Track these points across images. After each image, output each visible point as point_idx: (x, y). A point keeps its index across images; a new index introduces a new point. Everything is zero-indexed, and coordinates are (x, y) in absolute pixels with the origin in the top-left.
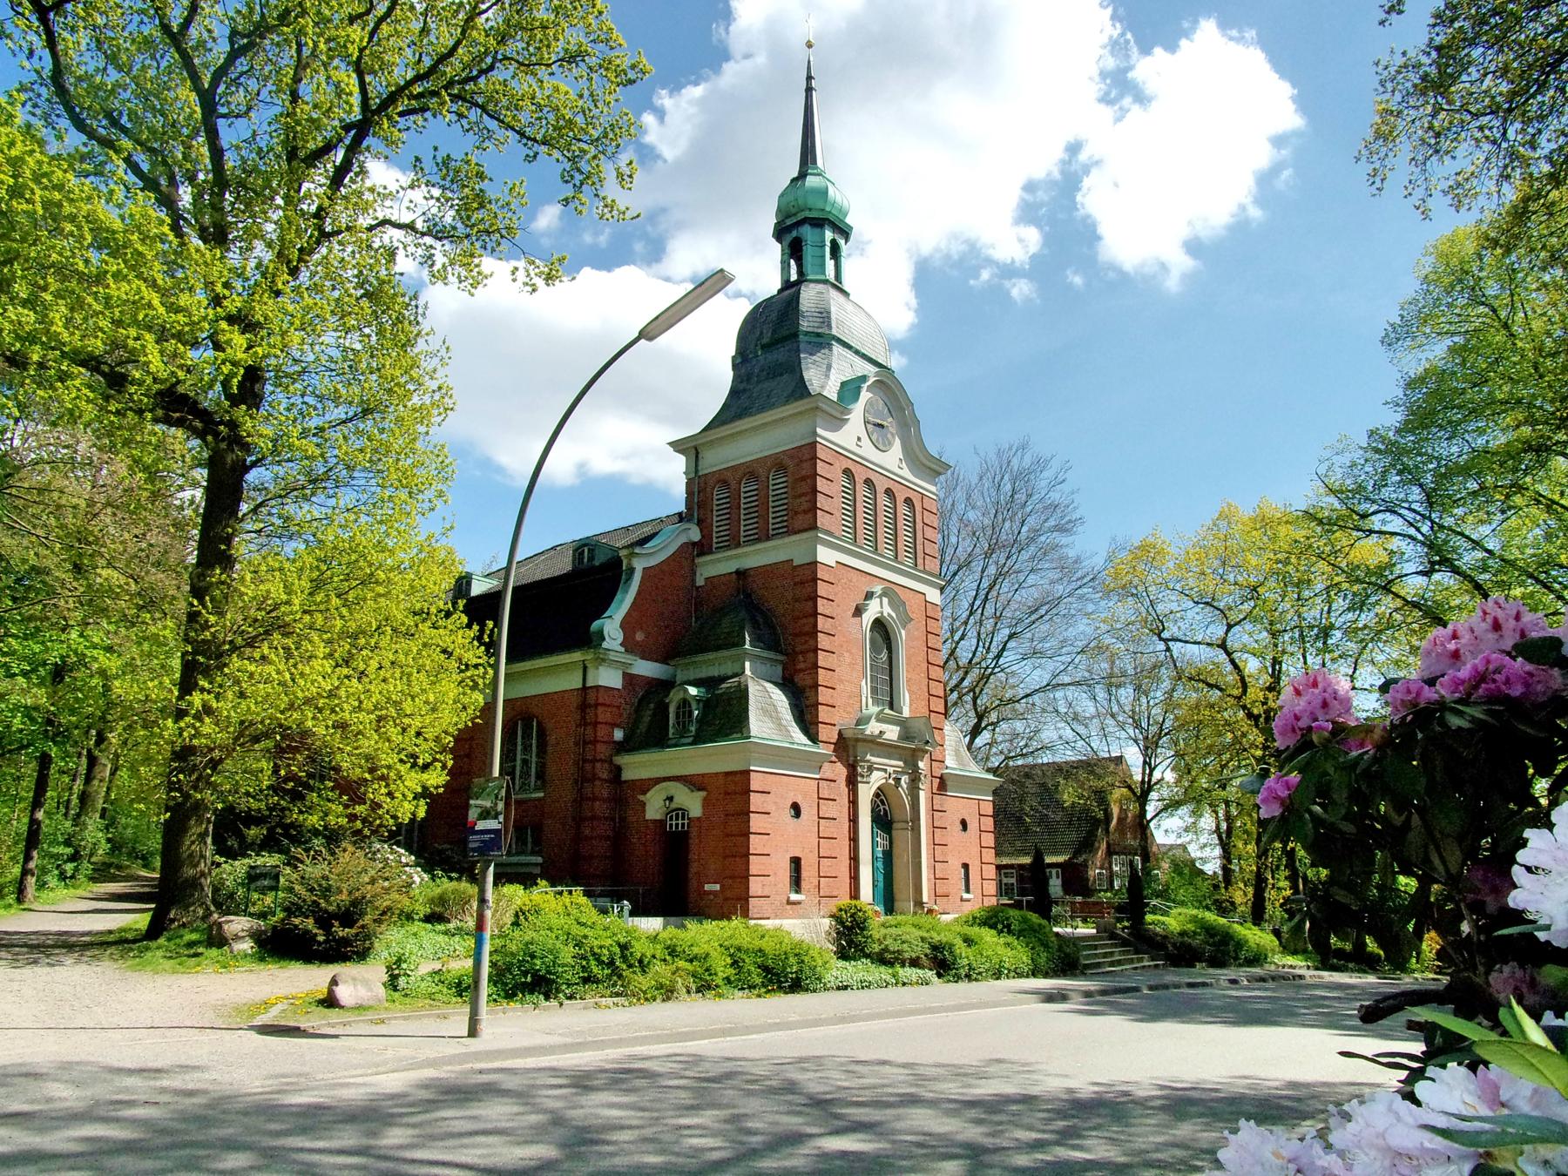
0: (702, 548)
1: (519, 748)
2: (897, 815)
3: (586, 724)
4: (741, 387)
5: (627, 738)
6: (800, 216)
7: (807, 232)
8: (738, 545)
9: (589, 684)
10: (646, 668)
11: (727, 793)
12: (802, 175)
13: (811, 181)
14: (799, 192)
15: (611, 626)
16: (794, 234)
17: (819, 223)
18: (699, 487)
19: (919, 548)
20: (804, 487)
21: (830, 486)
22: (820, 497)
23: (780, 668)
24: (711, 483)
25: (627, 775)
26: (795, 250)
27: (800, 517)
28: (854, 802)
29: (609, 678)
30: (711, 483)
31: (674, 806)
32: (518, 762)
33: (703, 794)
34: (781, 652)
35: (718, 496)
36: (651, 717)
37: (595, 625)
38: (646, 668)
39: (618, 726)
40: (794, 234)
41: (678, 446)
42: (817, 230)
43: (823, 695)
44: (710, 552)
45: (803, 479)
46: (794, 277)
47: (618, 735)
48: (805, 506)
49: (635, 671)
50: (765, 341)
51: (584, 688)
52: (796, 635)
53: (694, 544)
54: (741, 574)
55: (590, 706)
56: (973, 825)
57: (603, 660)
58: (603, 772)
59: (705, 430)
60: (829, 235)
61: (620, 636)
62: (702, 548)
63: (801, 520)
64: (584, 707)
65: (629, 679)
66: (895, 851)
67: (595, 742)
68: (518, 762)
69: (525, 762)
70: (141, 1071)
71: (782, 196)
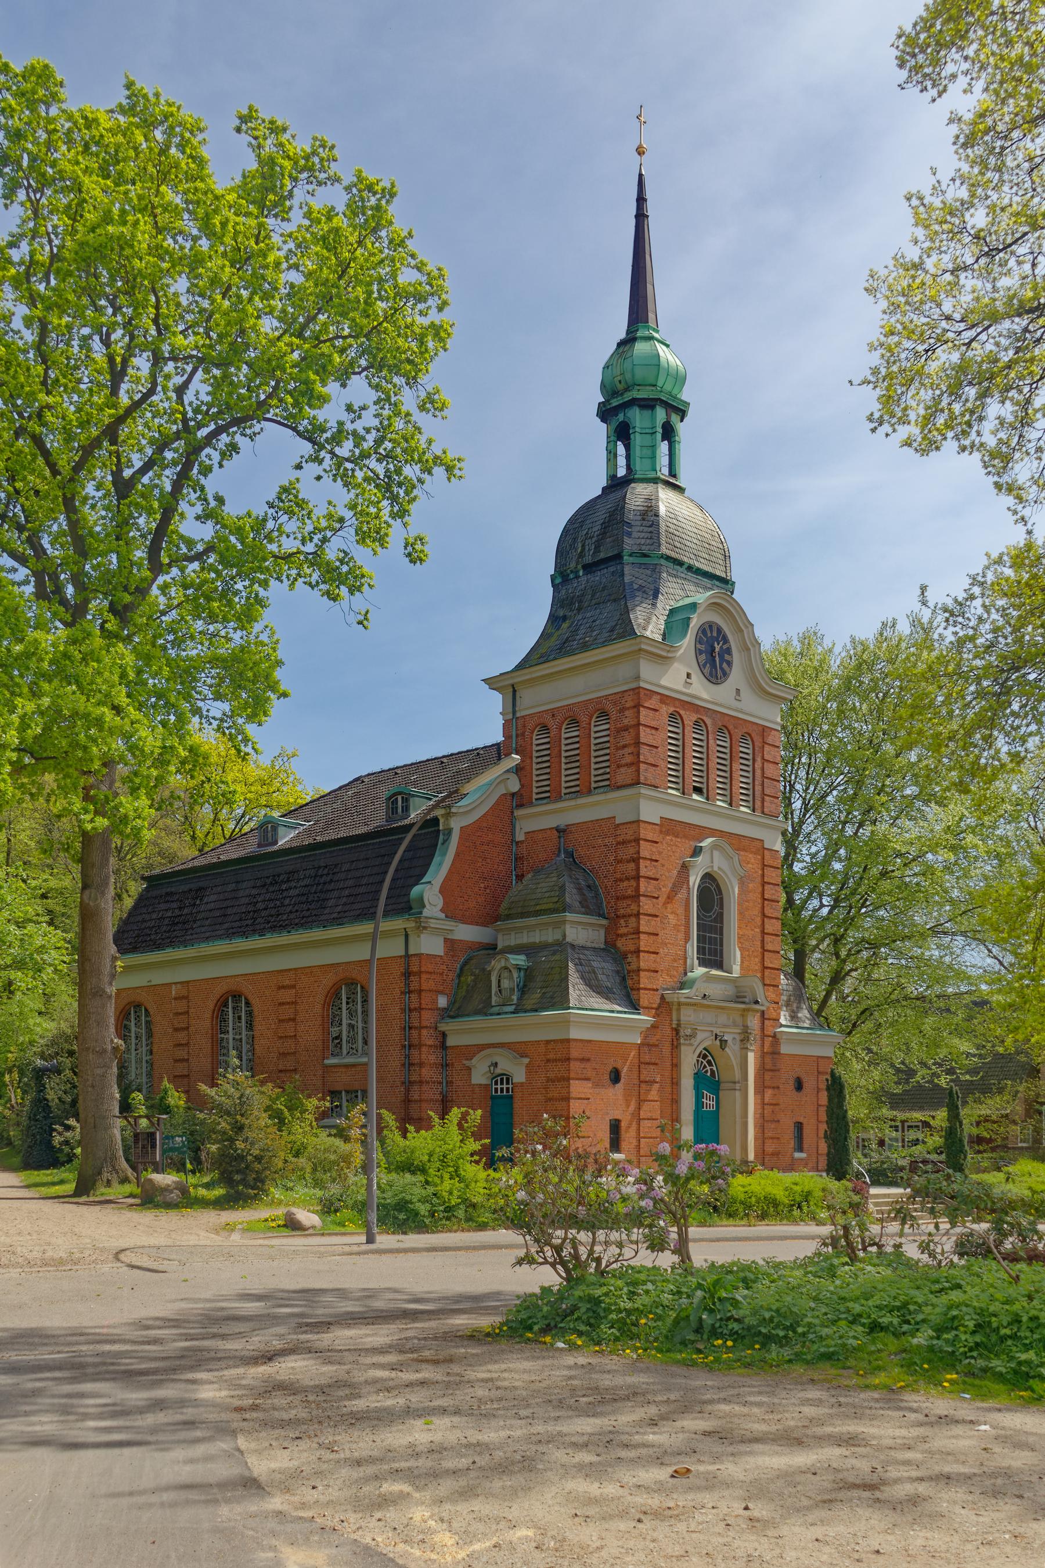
0: (519, 800)
1: (344, 1012)
2: (724, 1076)
3: (410, 992)
4: (561, 613)
5: (452, 1003)
6: (628, 396)
7: (637, 418)
8: (559, 798)
9: (411, 952)
10: (467, 933)
11: (548, 1061)
12: (628, 342)
13: (640, 347)
14: (627, 365)
15: (430, 892)
16: (621, 417)
17: (648, 405)
18: (517, 727)
19: (758, 788)
20: (627, 738)
21: (657, 734)
22: (644, 750)
23: (602, 932)
24: (530, 726)
25: (451, 1042)
26: (622, 433)
27: (623, 770)
28: (676, 1066)
29: (430, 945)
30: (530, 726)
31: (498, 1071)
32: (344, 1027)
33: (526, 1061)
34: (602, 915)
35: (537, 740)
36: (470, 984)
37: (416, 890)
38: (467, 933)
39: (442, 992)
40: (621, 417)
41: (492, 683)
42: (647, 413)
43: (645, 961)
44: (531, 804)
45: (626, 729)
46: (621, 472)
47: (442, 1002)
48: (628, 759)
49: (457, 936)
50: (588, 559)
51: (407, 956)
52: (618, 898)
53: (513, 795)
54: (561, 831)
55: (415, 974)
56: (809, 1083)
57: (425, 928)
58: (428, 1038)
59: (520, 667)
60: (661, 414)
61: (440, 903)
62: (519, 800)
63: (624, 775)
64: (407, 974)
65: (451, 944)
66: (722, 1111)
67: (420, 1009)
68: (344, 1027)
69: (351, 1026)
70: (718, 1240)
71: (606, 367)
